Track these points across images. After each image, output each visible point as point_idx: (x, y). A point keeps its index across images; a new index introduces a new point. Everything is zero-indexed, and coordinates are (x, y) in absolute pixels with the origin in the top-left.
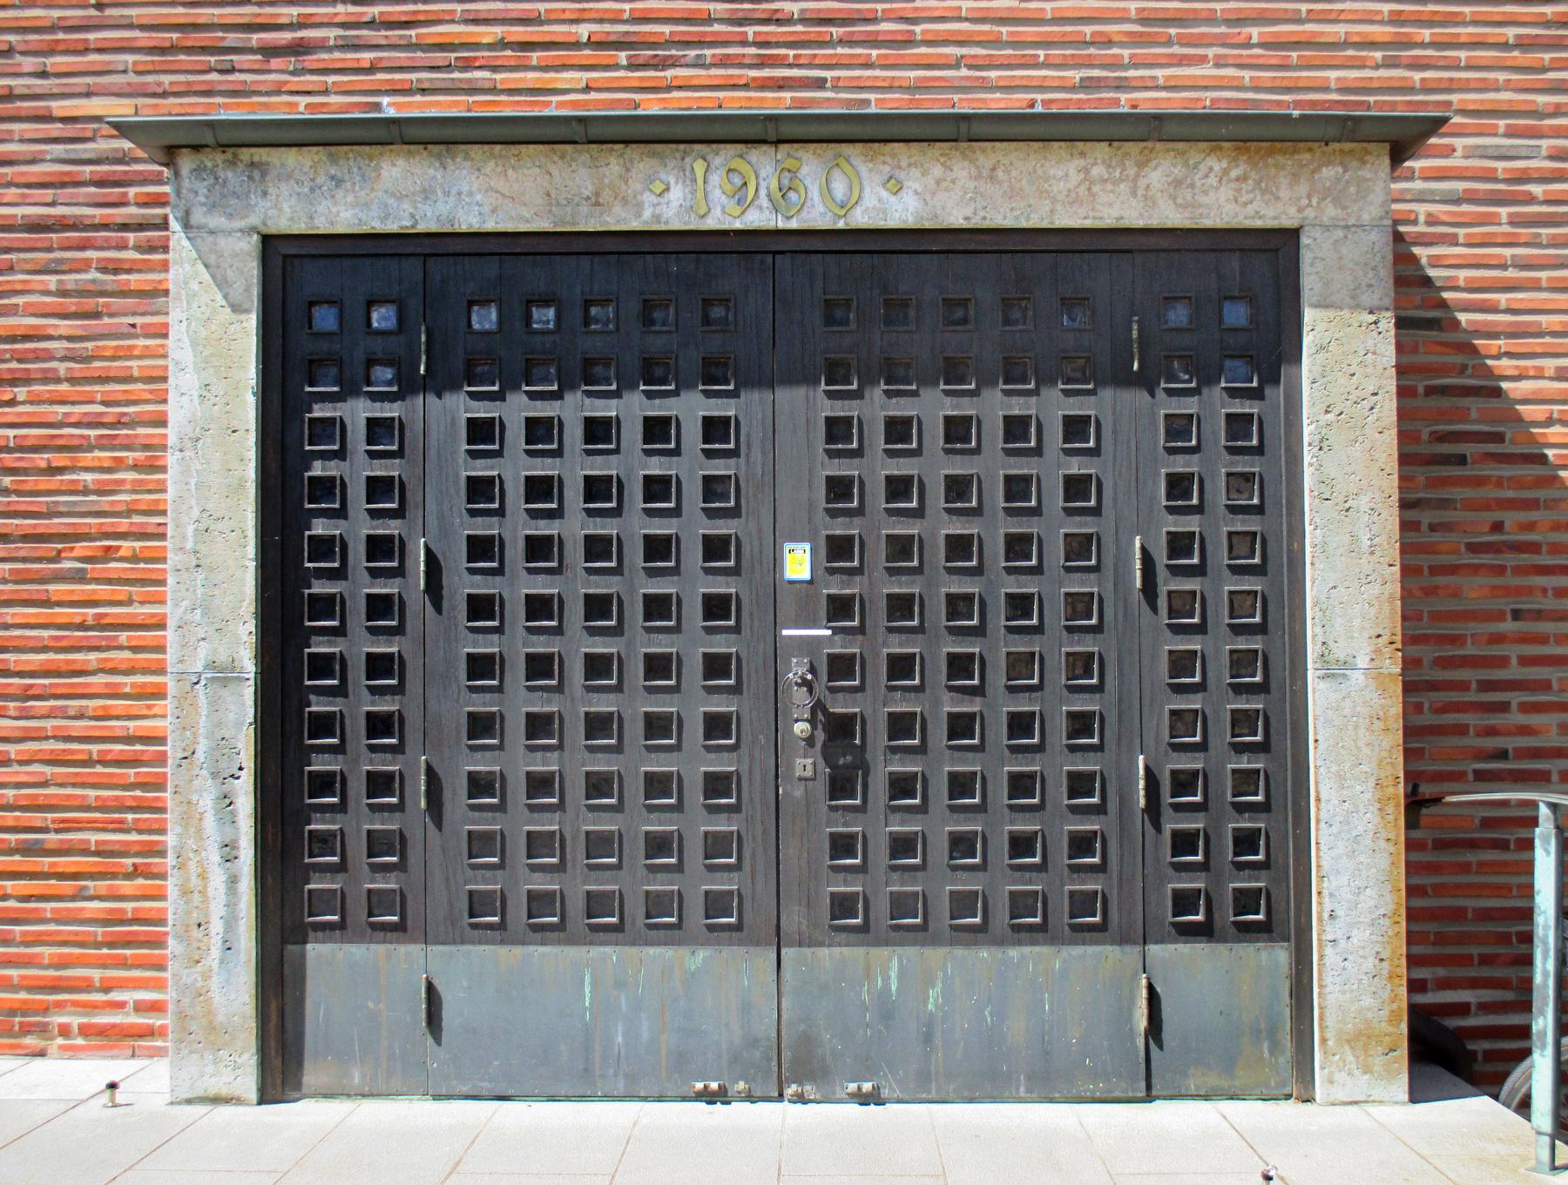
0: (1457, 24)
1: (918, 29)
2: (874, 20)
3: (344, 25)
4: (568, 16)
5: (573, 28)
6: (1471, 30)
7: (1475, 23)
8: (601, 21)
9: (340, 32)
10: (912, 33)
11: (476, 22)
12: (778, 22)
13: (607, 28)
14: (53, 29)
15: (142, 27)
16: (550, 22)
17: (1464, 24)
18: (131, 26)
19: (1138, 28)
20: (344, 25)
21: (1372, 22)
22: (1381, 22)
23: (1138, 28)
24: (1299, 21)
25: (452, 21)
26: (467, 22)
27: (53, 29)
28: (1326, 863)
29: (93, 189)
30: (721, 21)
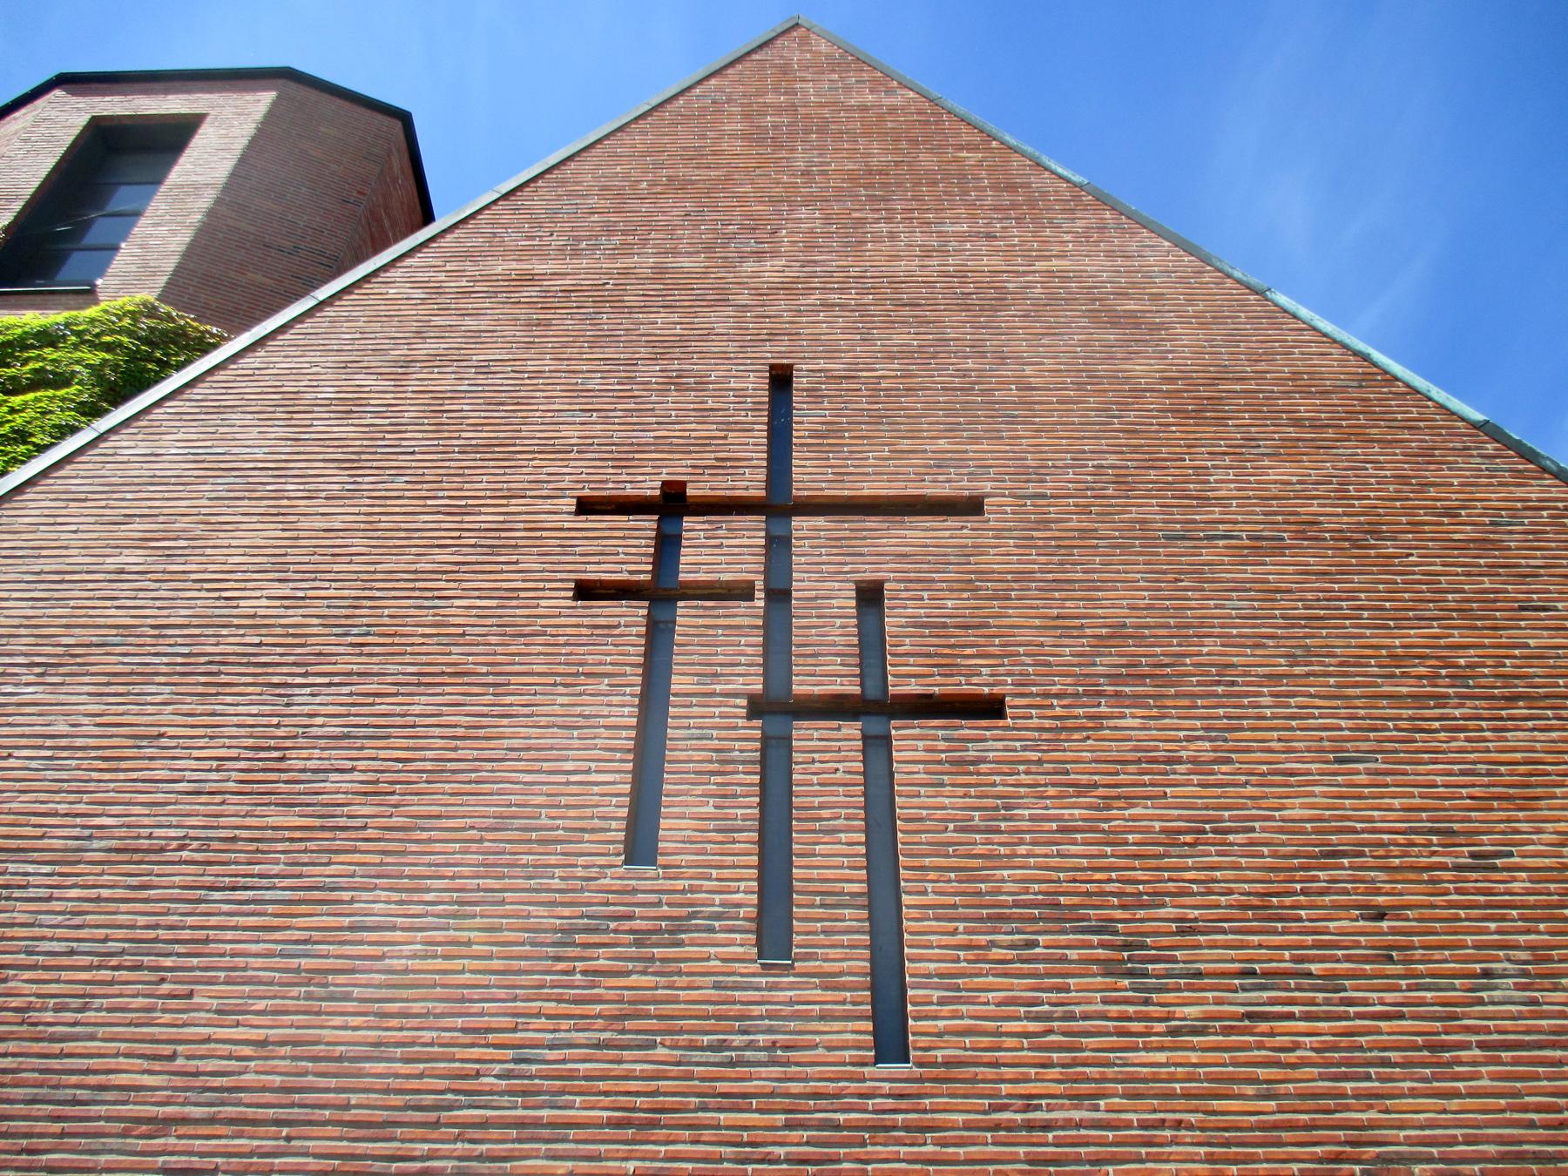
0: (1254, 1162)
1: (742, 911)
2: (838, 1161)
3: (460, 1158)
4: (620, 1155)
5: (624, 1164)
6: (1265, 1165)
7: (1268, 1161)
8: (643, 1159)
9: (456, 1163)
10: (865, 1171)
11: (554, 1158)
12: (770, 1162)
13: (648, 1164)
14: (251, 1154)
15: (315, 1156)
16: (607, 1159)
17: (1261, 1161)
18: (306, 1155)
19: (1026, 1167)
20: (460, 1158)
21: (1194, 1161)
22: (1200, 1161)
23: (1026, 1167)
24: (1141, 1161)
25: (537, 1157)
26: (548, 1158)
27: (251, 1154)
28: (398, 285)
29: (36, 1075)
30: (729, 1160)
